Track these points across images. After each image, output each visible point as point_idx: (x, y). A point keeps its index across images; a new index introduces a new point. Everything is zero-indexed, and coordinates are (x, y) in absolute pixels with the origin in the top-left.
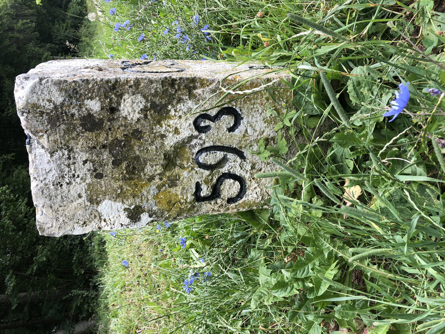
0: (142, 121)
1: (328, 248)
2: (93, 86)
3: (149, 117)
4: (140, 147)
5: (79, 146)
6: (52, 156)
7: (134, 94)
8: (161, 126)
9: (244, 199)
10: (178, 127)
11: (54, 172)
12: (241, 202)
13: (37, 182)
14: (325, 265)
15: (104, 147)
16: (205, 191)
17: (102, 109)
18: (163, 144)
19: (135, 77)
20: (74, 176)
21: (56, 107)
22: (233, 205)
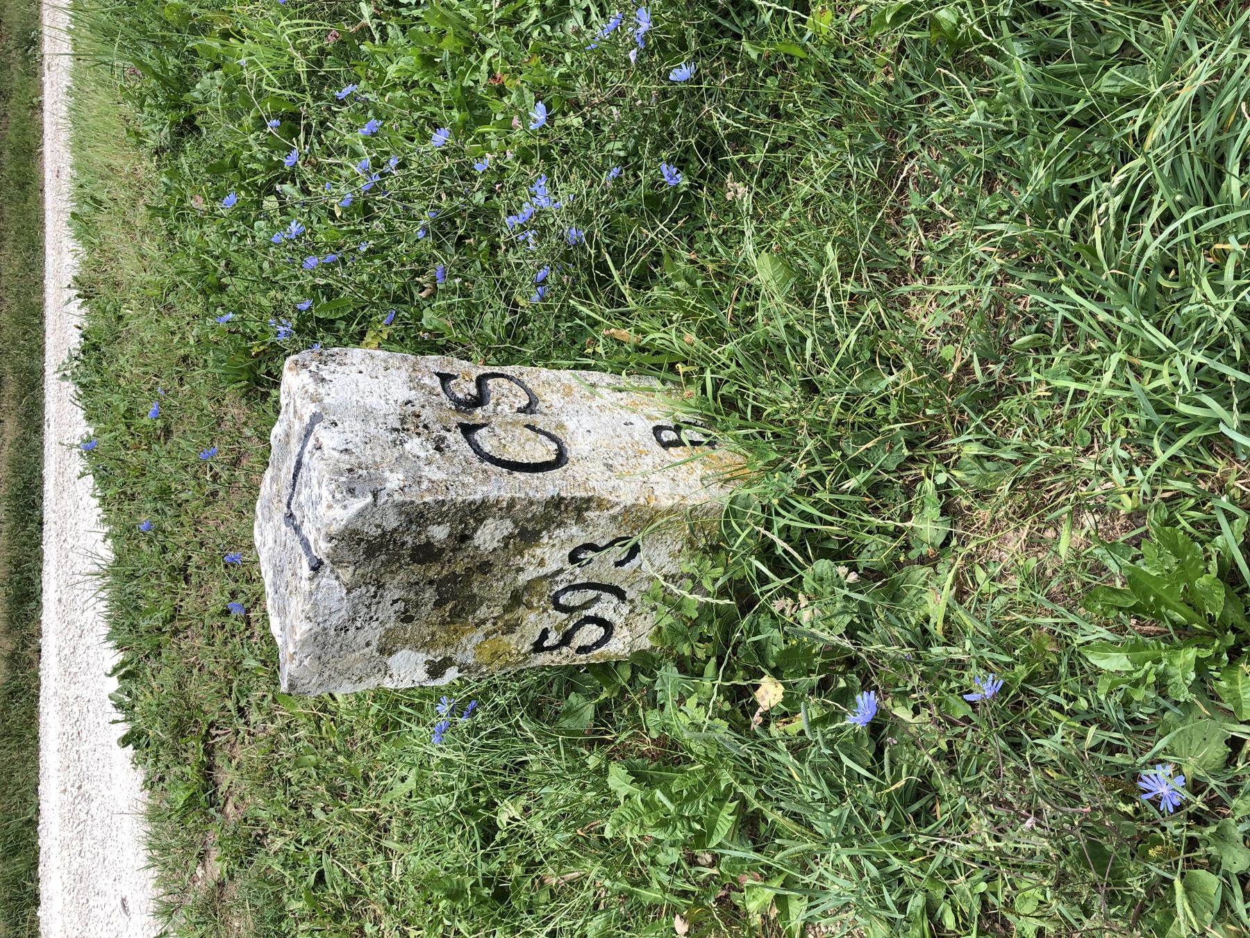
0: (499, 552)
2: (449, 509)
3: (511, 546)
4: (481, 583)
5: (395, 582)
6: (349, 592)
7: (502, 518)
8: (523, 557)
9: (602, 649)
10: (546, 557)
11: (343, 612)
12: (596, 652)
14: (720, 800)
15: (431, 582)
16: (553, 639)
17: (450, 536)
18: (515, 579)
20: (371, 618)
21: (384, 534)
22: (583, 656)
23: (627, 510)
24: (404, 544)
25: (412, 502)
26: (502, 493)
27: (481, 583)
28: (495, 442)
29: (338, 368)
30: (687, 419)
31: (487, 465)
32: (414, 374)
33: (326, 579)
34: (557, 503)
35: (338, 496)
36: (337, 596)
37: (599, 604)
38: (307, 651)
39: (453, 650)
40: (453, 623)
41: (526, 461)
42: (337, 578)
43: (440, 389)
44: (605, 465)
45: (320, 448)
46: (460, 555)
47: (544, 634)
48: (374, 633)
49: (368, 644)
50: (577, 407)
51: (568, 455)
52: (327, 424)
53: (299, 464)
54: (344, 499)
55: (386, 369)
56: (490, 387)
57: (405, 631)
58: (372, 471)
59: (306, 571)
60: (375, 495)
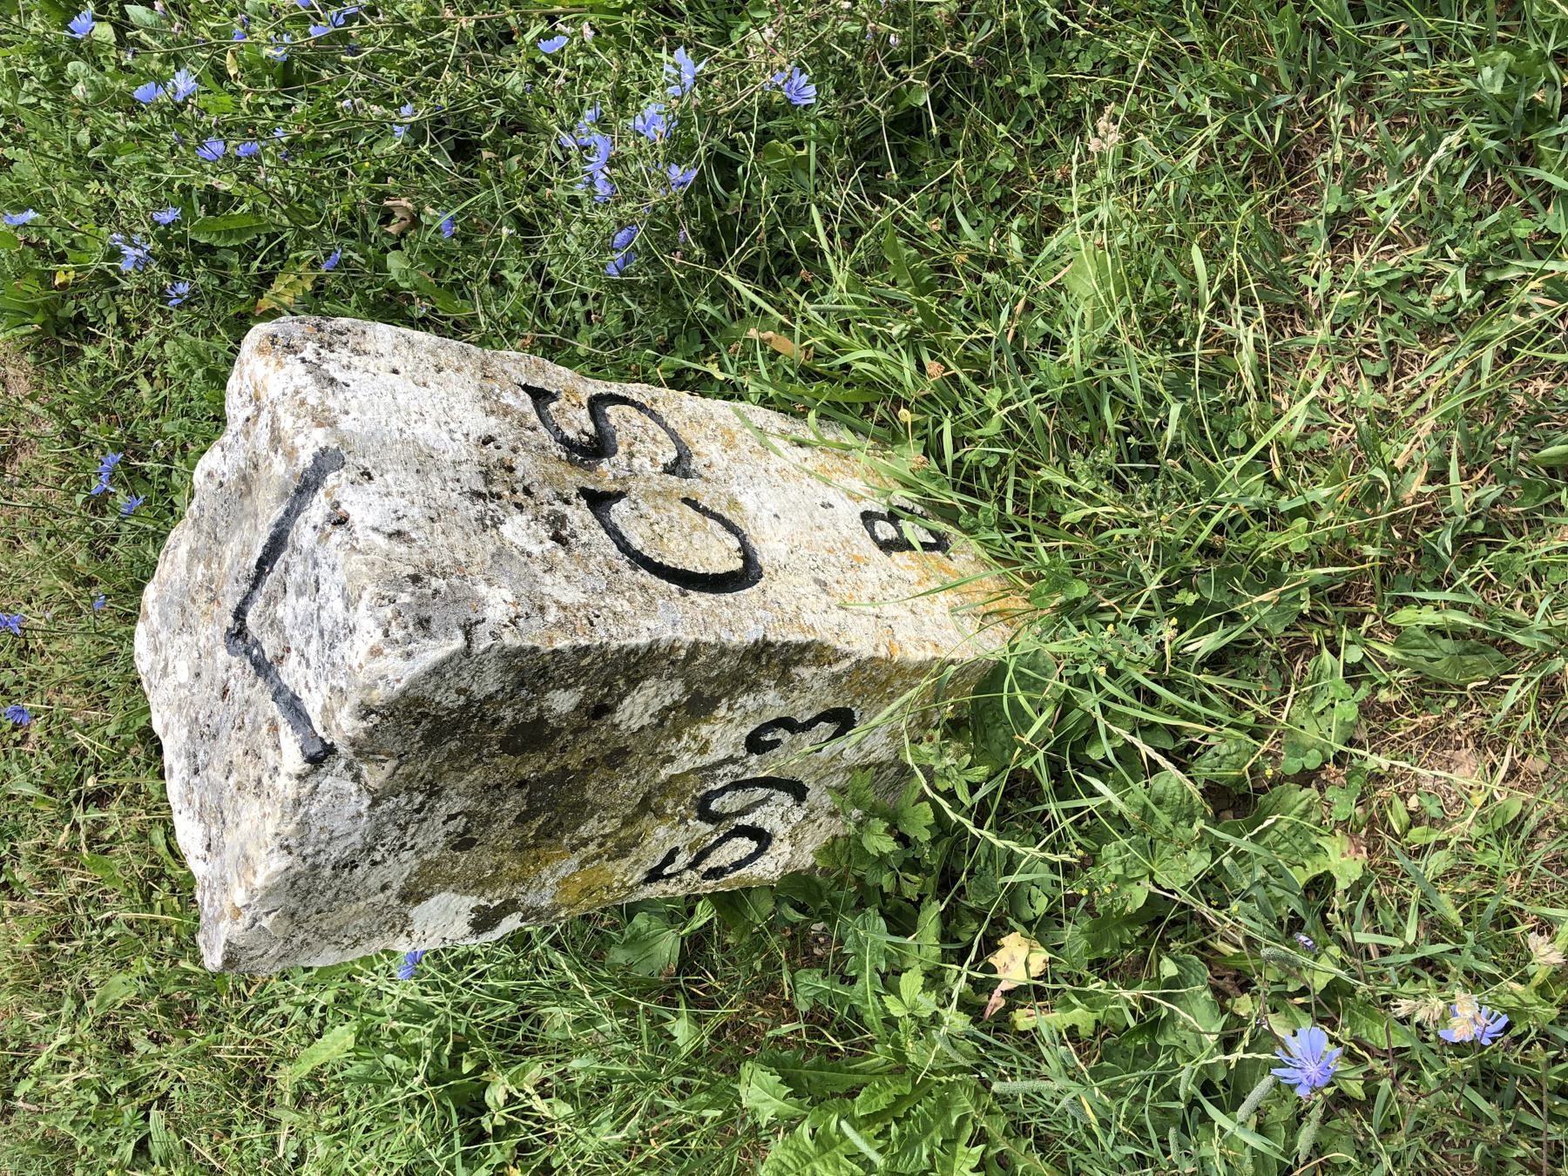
0: (648, 732)
1: (966, 1108)
3: (668, 724)
5: (462, 785)
6: (375, 803)
9: (743, 871)
13: (291, 858)
15: (522, 784)
17: (578, 707)
19: (691, 638)
21: (469, 704)
22: (709, 883)
23: (860, 665)
24: (496, 721)
25: (535, 649)
26: (680, 634)
27: (603, 782)
28: (643, 527)
29: (355, 360)
30: (907, 504)
31: (644, 576)
32: (485, 383)
33: (333, 780)
34: (760, 652)
35: (397, 633)
36: (350, 810)
37: (765, 809)
38: (273, 903)
39: (522, 889)
40: (536, 846)
41: (701, 571)
42: (357, 778)
43: (534, 418)
44: (817, 581)
45: (342, 521)
46: (583, 739)
47: (670, 858)
48: (399, 870)
49: (384, 888)
50: (750, 470)
51: (760, 560)
52: (354, 475)
53: (277, 544)
54: (409, 639)
55: (440, 370)
56: (613, 421)
57: (455, 863)
58: (455, 581)
59: (293, 759)
60: (468, 630)
